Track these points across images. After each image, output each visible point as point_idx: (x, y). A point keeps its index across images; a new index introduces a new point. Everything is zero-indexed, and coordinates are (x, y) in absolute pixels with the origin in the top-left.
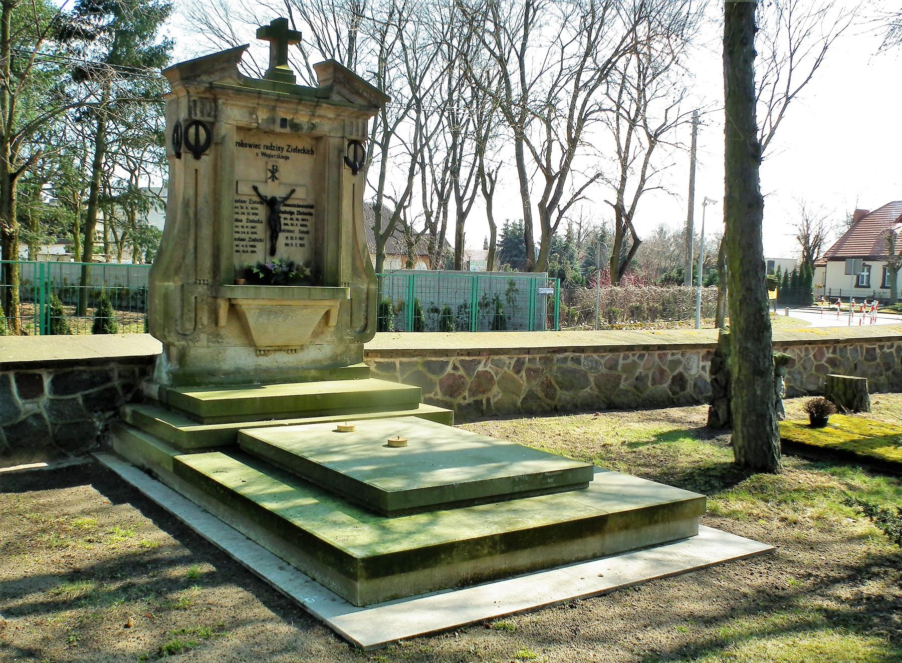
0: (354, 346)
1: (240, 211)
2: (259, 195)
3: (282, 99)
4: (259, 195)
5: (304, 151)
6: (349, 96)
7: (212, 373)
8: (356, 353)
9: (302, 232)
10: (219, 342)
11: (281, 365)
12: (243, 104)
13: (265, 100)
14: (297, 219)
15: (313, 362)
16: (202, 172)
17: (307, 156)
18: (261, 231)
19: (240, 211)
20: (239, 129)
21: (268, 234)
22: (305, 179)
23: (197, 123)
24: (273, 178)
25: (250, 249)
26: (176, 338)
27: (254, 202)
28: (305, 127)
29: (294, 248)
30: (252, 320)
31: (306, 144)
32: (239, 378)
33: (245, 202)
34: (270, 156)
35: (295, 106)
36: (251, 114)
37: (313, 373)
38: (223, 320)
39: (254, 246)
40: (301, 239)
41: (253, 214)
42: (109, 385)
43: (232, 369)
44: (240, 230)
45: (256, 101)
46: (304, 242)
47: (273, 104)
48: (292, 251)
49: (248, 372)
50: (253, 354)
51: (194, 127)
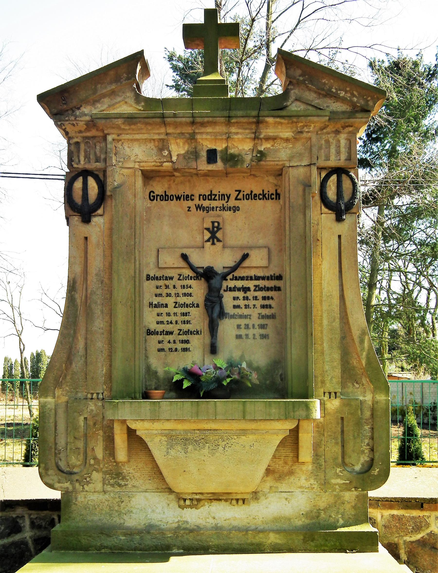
0: (350, 496)
1: (165, 291)
3: (198, 120)
5: (264, 196)
6: (317, 102)
7: (105, 531)
8: (354, 507)
9: (263, 317)
10: (120, 485)
11: (221, 523)
12: (146, 136)
13: (176, 125)
14: (255, 298)
15: (276, 520)
16: (94, 239)
17: (269, 204)
18: (198, 318)
20: (148, 176)
21: (207, 322)
22: (267, 239)
23: (85, 173)
25: (180, 346)
26: (56, 478)
28: (248, 158)
29: (250, 341)
30: (158, 453)
31: (266, 185)
32: (148, 541)
33: (171, 278)
34: (207, 209)
35: (224, 129)
36: (161, 150)
37: (273, 538)
38: (121, 454)
39: (187, 342)
40: (262, 327)
41: (185, 295)
42: (17, 537)
43: (141, 526)
45: (163, 130)
46: (268, 331)
47: (189, 130)
48: (243, 344)
49: (162, 532)
50: (174, 504)
51: (81, 179)
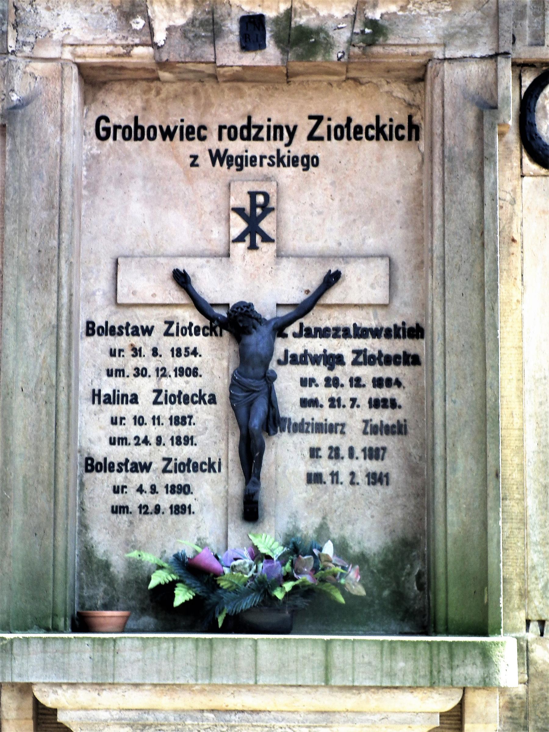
2: (198, 303)
4: (198, 303)
5: (380, 132)
14: (356, 382)
17: (392, 149)
18: (212, 432)
19: (130, 363)
24: (253, 234)
25: (166, 500)
27: (185, 331)
28: (342, 37)
29: (343, 489)
31: (385, 103)
33: (148, 331)
34: (240, 162)
39: (185, 489)
40: (373, 454)
44: (131, 431)
48: (327, 500)
